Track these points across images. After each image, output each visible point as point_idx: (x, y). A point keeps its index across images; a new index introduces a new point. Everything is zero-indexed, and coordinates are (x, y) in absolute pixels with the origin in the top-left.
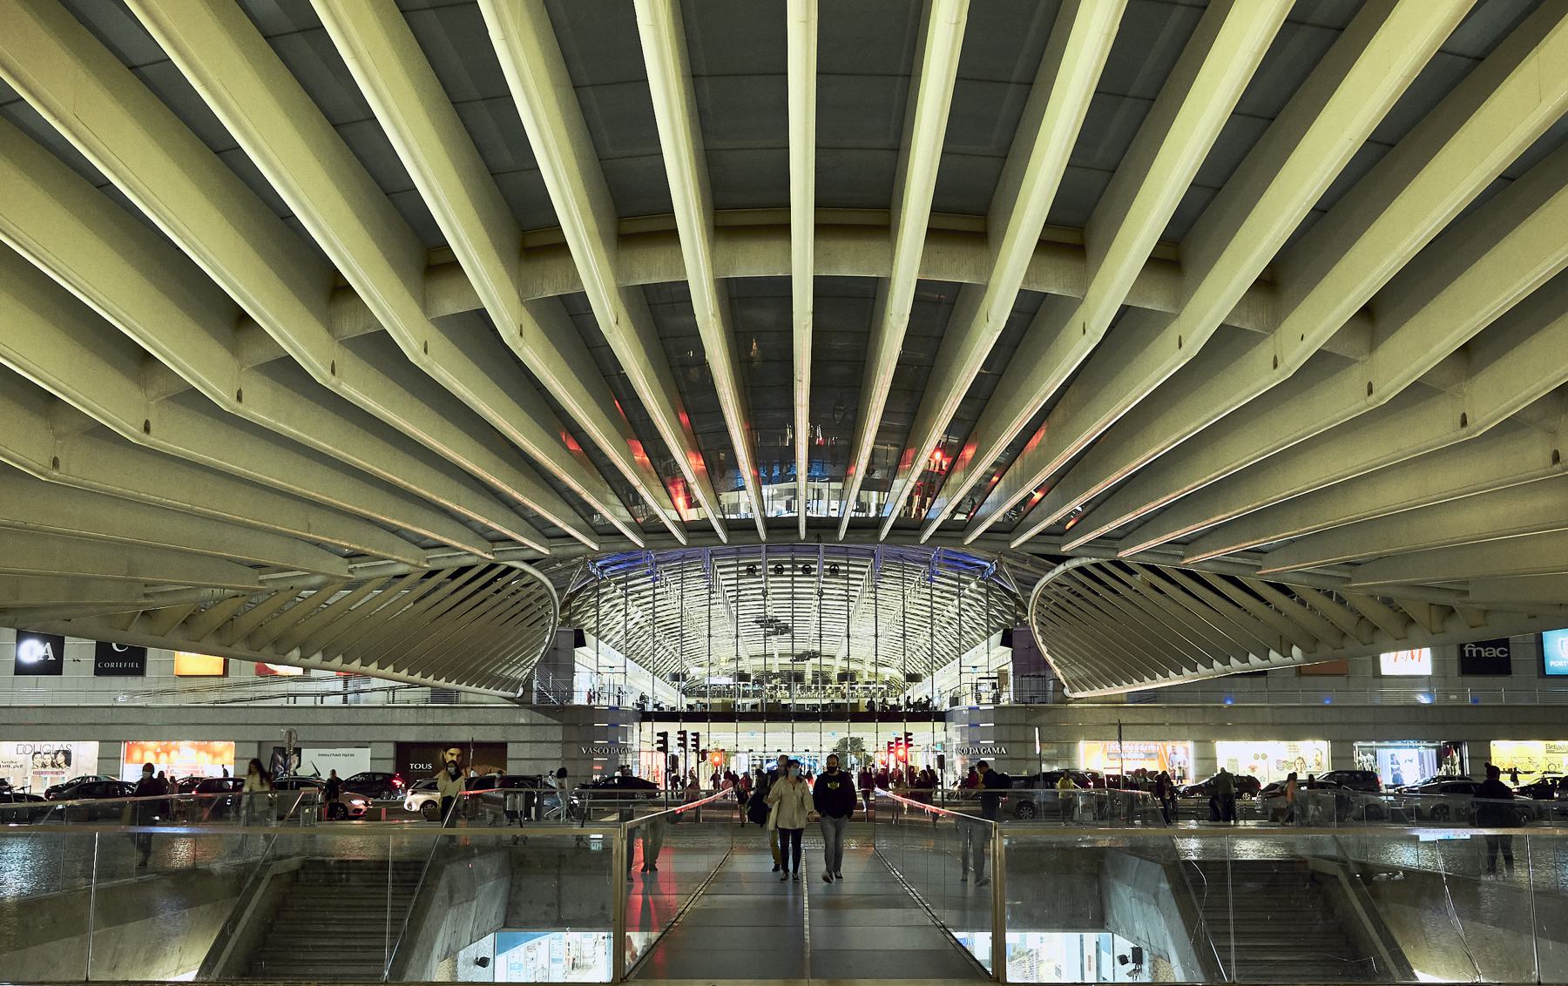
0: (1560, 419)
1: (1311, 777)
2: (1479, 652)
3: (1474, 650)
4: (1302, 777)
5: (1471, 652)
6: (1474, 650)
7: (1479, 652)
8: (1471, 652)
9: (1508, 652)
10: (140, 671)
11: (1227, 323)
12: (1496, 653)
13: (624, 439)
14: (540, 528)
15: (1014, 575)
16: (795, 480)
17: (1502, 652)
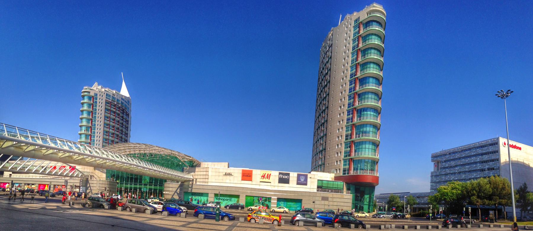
0: (27, 189)
1: (515, 145)
2: (282, 177)
3: (281, 176)
4: (516, 146)
5: (281, 176)
6: (281, 176)
7: (282, 177)
8: (281, 176)
9: (289, 177)
10: (251, 180)
11: (336, 176)
12: (286, 177)
13: (176, 216)
14: (329, 182)
15: (49, 138)
16: (375, 161)
17: (288, 177)
